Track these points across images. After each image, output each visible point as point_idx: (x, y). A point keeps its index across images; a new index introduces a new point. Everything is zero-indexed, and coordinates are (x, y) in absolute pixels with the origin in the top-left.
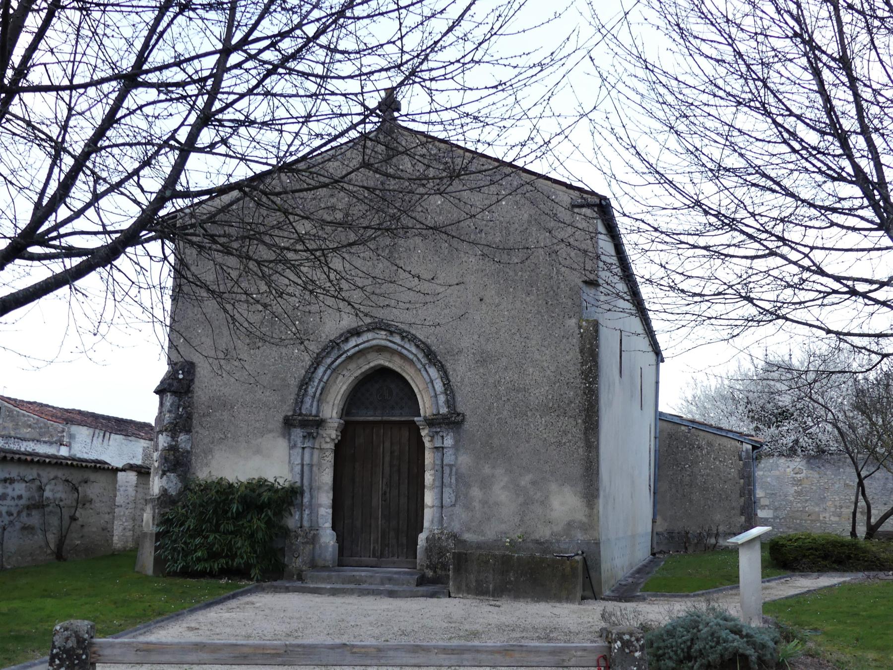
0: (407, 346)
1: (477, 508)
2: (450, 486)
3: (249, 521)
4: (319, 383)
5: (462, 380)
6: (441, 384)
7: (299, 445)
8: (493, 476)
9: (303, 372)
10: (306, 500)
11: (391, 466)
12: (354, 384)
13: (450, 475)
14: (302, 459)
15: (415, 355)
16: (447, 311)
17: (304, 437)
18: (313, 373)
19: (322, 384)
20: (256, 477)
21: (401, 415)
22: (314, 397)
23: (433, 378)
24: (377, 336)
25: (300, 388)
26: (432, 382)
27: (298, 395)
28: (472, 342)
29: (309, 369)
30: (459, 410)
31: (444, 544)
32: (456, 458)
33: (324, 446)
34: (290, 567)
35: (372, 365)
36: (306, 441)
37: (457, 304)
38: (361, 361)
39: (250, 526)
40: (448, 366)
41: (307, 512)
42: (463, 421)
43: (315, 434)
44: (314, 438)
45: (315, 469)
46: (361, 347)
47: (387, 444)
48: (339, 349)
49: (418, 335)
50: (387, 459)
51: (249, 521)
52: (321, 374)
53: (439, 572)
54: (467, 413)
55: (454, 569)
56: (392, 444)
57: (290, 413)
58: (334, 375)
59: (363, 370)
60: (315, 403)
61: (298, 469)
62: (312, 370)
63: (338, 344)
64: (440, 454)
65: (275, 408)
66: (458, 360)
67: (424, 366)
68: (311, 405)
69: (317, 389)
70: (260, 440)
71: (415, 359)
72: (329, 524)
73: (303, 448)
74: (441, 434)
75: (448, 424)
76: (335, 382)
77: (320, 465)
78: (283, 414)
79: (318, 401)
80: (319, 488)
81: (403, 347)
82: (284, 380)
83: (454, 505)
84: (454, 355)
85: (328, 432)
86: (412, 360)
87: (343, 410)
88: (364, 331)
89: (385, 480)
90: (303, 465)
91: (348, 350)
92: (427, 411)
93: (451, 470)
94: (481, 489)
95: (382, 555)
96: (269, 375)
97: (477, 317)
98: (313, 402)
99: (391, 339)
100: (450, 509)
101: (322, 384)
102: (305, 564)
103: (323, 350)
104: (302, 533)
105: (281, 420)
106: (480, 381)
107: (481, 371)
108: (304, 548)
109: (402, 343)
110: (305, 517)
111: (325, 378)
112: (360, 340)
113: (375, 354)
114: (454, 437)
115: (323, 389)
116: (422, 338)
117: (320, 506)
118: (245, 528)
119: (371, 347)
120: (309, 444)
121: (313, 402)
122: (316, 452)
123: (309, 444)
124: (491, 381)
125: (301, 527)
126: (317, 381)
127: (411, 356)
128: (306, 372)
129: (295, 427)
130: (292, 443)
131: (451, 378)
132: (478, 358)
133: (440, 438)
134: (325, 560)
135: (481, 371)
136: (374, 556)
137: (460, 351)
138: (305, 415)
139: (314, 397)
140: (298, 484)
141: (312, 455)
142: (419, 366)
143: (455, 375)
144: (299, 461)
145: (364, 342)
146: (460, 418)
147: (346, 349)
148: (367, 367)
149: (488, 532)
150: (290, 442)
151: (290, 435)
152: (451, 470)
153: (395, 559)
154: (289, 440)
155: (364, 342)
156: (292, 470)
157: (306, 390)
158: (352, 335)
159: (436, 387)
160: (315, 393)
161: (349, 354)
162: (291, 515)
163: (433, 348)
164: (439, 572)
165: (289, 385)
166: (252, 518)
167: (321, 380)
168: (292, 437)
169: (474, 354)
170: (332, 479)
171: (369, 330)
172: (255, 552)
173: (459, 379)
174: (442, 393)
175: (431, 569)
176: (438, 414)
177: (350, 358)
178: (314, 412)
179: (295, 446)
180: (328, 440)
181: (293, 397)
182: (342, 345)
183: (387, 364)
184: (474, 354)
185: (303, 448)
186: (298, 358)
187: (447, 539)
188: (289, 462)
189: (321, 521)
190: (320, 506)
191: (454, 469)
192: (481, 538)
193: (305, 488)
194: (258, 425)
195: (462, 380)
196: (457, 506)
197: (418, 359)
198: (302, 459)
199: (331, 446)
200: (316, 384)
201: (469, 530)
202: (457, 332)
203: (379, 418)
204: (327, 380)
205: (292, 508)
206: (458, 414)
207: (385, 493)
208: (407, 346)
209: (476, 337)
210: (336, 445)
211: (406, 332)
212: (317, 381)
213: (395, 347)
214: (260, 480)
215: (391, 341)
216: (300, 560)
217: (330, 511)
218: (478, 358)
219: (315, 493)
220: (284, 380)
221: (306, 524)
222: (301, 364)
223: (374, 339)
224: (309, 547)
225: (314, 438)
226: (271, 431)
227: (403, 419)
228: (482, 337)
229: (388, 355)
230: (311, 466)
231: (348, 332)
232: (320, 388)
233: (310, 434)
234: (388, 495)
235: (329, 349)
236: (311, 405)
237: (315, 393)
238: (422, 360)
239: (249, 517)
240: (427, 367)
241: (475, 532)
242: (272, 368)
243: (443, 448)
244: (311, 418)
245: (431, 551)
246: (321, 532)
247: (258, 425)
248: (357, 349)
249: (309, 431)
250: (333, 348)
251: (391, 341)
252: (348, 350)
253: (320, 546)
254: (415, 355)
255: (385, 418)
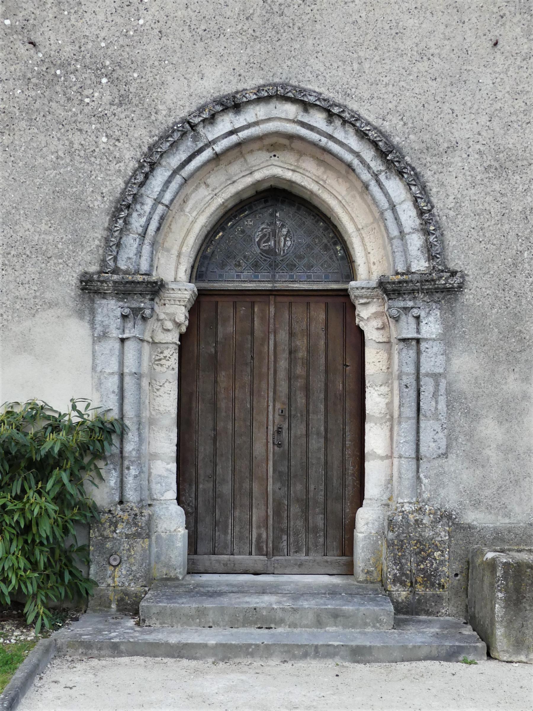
0: (339, 134)
1: (493, 461)
2: (436, 416)
3: (18, 498)
4: (154, 208)
5: (458, 205)
6: (413, 213)
7: (115, 333)
8: (525, 397)
9: (120, 183)
10: (130, 447)
11: (290, 378)
12: (216, 218)
13: (435, 395)
14: (121, 363)
15: (357, 155)
16: (423, 66)
17: (124, 317)
18: (142, 185)
19: (160, 209)
20: (23, 400)
21: (309, 280)
22: (143, 235)
23: (396, 200)
24: (275, 113)
25: (115, 217)
26: (393, 207)
27: (109, 230)
28: (477, 129)
29: (134, 175)
30: (452, 266)
31: (428, 533)
32: (448, 360)
33: (161, 337)
34: (103, 586)
35: (258, 176)
36: (130, 325)
37: (444, 53)
38: (235, 168)
39: (22, 510)
40: (427, 175)
41: (133, 471)
42: (461, 286)
43: (148, 312)
44: (144, 319)
45: (145, 383)
46: (243, 134)
47: (283, 336)
48: (196, 138)
49: (363, 113)
50: (283, 364)
51: (18, 498)
52: (157, 189)
53: (420, 589)
54: (471, 271)
55: (507, 600)
56: (291, 334)
57: (94, 268)
58: (188, 189)
59: (240, 186)
60: (146, 249)
61: (113, 383)
62: (140, 178)
63: (193, 127)
64: (412, 353)
65: (61, 257)
66: (450, 164)
67: (376, 176)
68: (139, 254)
69: (149, 220)
70: (28, 323)
71: (356, 162)
72: (172, 494)
73: (123, 340)
74: (415, 312)
75: (429, 292)
76: (182, 210)
77: (153, 377)
78: (79, 270)
79: (153, 244)
80: (152, 422)
81: (331, 137)
82: (78, 199)
83: (445, 455)
84: (439, 155)
85: (170, 309)
86: (349, 166)
87: (193, 267)
88: (249, 102)
89: (278, 406)
90: (122, 376)
91: (214, 142)
92: (374, 268)
93: (437, 385)
94: (501, 423)
95: (276, 550)
96: (46, 189)
97: (487, 80)
98: (141, 245)
99: (306, 119)
100: (436, 463)
101: (160, 209)
102: (136, 579)
103: (164, 137)
104: (125, 516)
105: (74, 281)
106: (495, 208)
107: (497, 187)
108: (131, 546)
109: (329, 130)
110: (130, 482)
111: (167, 197)
112: (240, 120)
113: (263, 156)
114: (444, 321)
115: (162, 218)
116: (371, 118)
117: (154, 456)
118: (11, 513)
119: (260, 138)
120: (136, 332)
121: (141, 245)
122: (146, 348)
123: (136, 332)
124: (517, 207)
125: (121, 502)
126: (149, 203)
127: (348, 157)
128: (127, 183)
129: (104, 296)
130: (99, 329)
131: (434, 200)
132: (489, 160)
133: (412, 322)
134: (168, 565)
135: (497, 187)
136: (260, 552)
137: (453, 147)
138: (126, 272)
139: (143, 235)
140: (114, 415)
141: (140, 353)
142: (366, 176)
143: (442, 195)
144: (115, 367)
145: (249, 126)
146: (455, 281)
147: (211, 138)
148: (249, 180)
149: (517, 509)
150: (93, 328)
151: (93, 312)
152: (437, 385)
153: (302, 557)
154: (92, 323)
155: (249, 126)
156: (99, 385)
157: (126, 222)
158: (226, 109)
159: (403, 218)
160: (146, 228)
161: (219, 148)
162: (101, 478)
163: (396, 140)
164: (420, 589)
165: (89, 210)
166: (24, 491)
167: (157, 201)
168: (99, 318)
169: (480, 152)
170: (367, 395)
171: (259, 100)
172: (34, 566)
173: (450, 202)
174: (415, 230)
175: (403, 584)
176: (408, 272)
177: (217, 157)
178: (144, 267)
179: (104, 336)
180: (169, 325)
181: (100, 233)
182: (201, 129)
183: (289, 175)
184: (480, 152)
185: (123, 340)
186: (107, 154)
187: (435, 522)
188: (94, 369)
189: (156, 488)
190: (154, 456)
191: (443, 384)
192: (502, 522)
193: (127, 422)
194: (22, 292)
195: (458, 205)
196: (452, 457)
197: (363, 161)
198: (121, 363)
199: (174, 337)
200: (147, 208)
201: (477, 504)
202: (446, 108)
203: (268, 286)
204: (172, 201)
205: (101, 464)
206: (453, 273)
207: (279, 431)
208: (339, 134)
209: (483, 119)
210: (182, 337)
211: (339, 106)
212: (149, 203)
213: (314, 136)
214: (33, 406)
215: (303, 124)
216: (123, 570)
217: (173, 467)
218: (489, 160)
219: (145, 431)
220: (78, 199)
221: (131, 495)
222: (113, 166)
223: (269, 120)
224: (140, 545)
225: (144, 319)
226: (51, 305)
227: (315, 287)
228: (496, 121)
229: (290, 158)
230: (138, 376)
231: (219, 102)
232: (156, 218)
233: (136, 311)
234: (285, 434)
235: (177, 136)
236: (139, 254)
237: (146, 228)
238: (372, 164)
239: (16, 488)
240: (382, 177)
241: (489, 508)
242: (52, 173)
243: (418, 341)
244: (140, 278)
245: (401, 549)
246: (158, 509)
247: (22, 292)
248: (234, 139)
249: (135, 305)
250: (184, 134)
251: (303, 124)
252: (214, 142)
253: (158, 537)
254: (357, 155)
255: (279, 286)
